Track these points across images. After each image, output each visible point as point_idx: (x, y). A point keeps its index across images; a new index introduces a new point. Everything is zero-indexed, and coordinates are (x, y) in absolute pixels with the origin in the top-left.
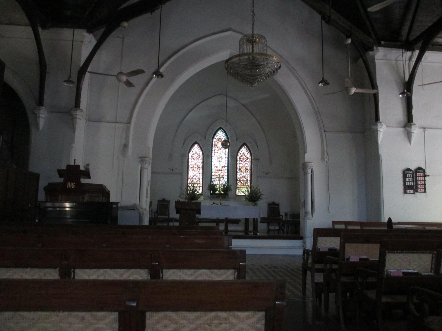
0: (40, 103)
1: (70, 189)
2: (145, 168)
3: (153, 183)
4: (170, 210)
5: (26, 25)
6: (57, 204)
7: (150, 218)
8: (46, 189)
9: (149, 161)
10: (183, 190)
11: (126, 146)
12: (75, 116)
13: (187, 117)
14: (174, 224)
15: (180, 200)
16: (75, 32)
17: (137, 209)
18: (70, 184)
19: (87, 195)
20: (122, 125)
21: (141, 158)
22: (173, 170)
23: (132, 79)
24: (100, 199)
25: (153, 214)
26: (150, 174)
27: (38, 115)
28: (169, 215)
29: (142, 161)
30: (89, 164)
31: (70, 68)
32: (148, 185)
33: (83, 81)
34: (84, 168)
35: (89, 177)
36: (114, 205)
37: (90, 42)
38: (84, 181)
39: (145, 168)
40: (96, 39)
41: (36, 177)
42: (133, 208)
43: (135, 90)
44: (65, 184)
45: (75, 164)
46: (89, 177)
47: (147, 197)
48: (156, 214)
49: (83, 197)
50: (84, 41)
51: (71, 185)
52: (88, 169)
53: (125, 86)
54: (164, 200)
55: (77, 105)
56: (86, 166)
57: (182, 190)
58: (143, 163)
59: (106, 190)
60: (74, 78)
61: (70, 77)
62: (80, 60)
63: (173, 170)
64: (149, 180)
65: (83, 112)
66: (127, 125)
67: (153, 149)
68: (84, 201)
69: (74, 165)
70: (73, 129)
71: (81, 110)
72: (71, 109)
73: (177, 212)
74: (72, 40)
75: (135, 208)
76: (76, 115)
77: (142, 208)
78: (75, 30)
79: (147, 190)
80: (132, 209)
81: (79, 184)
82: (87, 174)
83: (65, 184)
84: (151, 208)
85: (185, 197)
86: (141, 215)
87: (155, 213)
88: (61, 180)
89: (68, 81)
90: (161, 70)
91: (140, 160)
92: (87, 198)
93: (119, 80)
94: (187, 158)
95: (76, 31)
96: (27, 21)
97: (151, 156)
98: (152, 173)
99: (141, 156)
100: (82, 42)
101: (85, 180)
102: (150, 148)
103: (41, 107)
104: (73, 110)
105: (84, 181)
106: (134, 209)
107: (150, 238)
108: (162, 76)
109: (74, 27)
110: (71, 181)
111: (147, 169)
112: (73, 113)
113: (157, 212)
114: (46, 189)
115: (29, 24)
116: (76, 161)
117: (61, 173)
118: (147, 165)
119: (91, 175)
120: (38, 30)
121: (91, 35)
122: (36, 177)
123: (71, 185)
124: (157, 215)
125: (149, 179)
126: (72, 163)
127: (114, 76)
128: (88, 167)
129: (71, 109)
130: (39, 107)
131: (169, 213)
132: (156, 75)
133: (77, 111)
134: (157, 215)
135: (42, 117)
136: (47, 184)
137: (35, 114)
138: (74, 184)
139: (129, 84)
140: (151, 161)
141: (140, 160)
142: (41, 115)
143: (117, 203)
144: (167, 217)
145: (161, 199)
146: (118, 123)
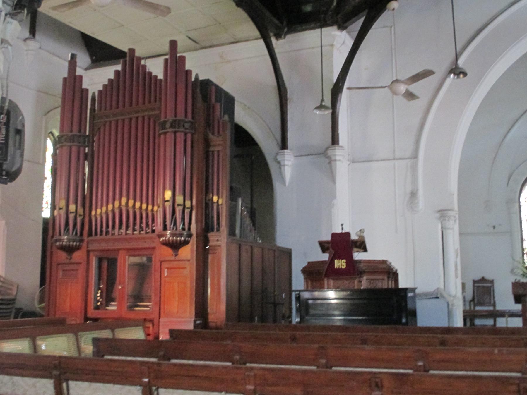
0: (284, 145)
1: (339, 270)
2: (449, 229)
3: (463, 251)
4: (495, 294)
5: (257, 39)
6: (317, 294)
7: (465, 312)
8: (305, 271)
9: (455, 217)
10: (517, 261)
11: (413, 195)
12: (333, 158)
13: (510, 134)
14: (507, 322)
15: (519, 281)
16: (323, 33)
17: (443, 297)
18: (339, 263)
19: (365, 278)
20: (404, 162)
21: (440, 212)
22: (494, 227)
23: (414, 88)
24: (385, 284)
25: (468, 304)
26: (457, 237)
27: (282, 163)
28: (494, 305)
29: (442, 216)
30: (364, 230)
31: (178, 106)
32: (457, 257)
33: (340, 103)
34: (358, 236)
35: (365, 250)
36: (410, 292)
37: (344, 43)
38: (358, 256)
39: (449, 229)
40: (352, 37)
41: (288, 253)
42: (436, 296)
43: (419, 104)
44: (331, 262)
45: (344, 232)
46: (365, 250)
47: (456, 277)
48: (472, 303)
49: (360, 282)
50: (335, 43)
51: (340, 264)
52: (363, 237)
53: (404, 100)
54: (483, 280)
55: (335, 140)
56: (359, 233)
57: (513, 260)
58: (445, 220)
59: (392, 269)
60: (328, 102)
61: (322, 100)
62: (332, 72)
63: (494, 227)
64: (456, 248)
65: (343, 150)
66: (413, 160)
67: (458, 195)
68: (362, 288)
69: (342, 234)
70: (332, 176)
71: (341, 147)
72: (327, 149)
73: (518, 299)
74: (320, 45)
75: (439, 296)
76: (335, 155)
77: (450, 296)
78: (323, 29)
79: (456, 266)
80: (434, 296)
81: (351, 262)
82: (362, 245)
83: (331, 262)
84: (464, 294)
85: (521, 273)
86: (450, 307)
87: (471, 301)
88: (325, 257)
89: (321, 107)
90: (461, 62)
91: (438, 215)
92: (364, 283)
93: (395, 93)
94: (517, 204)
95: (324, 29)
96: (257, 33)
97: (456, 207)
98: (461, 234)
99: (440, 208)
100: (332, 45)
101: (359, 254)
102: (453, 194)
103: (286, 151)
104: (330, 149)
105: (358, 256)
106: (437, 298)
107: (496, 351)
108: (465, 74)
109: (321, 27)
110: (340, 258)
111: (452, 229)
112: (330, 153)
113: (473, 300)
114: (305, 271)
115: (260, 36)
116: (344, 226)
117: (324, 246)
118: (452, 222)
119: (368, 246)
120: (271, 41)
121: (344, 32)
122: (288, 253)
123: (340, 264)
124: (475, 306)
125: (457, 245)
126: (339, 231)
127: (385, 87)
128: (362, 234)
129: (327, 149)
130: (283, 151)
131: (495, 303)
132: (455, 74)
133: (335, 149)
134: (475, 306)
135: (288, 165)
136: (306, 264)
137: (279, 163)
138: (344, 262)
139: (410, 96)
140: (457, 216)
141: (438, 215)
142: (286, 163)
143: (413, 290)
144: (491, 308)
145: (478, 277)
146: (397, 159)
